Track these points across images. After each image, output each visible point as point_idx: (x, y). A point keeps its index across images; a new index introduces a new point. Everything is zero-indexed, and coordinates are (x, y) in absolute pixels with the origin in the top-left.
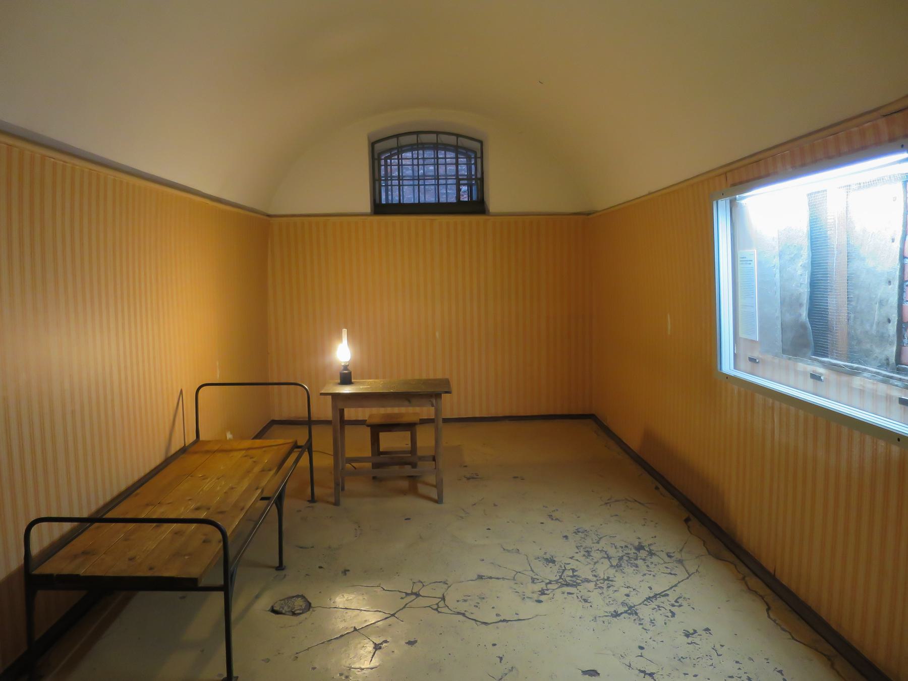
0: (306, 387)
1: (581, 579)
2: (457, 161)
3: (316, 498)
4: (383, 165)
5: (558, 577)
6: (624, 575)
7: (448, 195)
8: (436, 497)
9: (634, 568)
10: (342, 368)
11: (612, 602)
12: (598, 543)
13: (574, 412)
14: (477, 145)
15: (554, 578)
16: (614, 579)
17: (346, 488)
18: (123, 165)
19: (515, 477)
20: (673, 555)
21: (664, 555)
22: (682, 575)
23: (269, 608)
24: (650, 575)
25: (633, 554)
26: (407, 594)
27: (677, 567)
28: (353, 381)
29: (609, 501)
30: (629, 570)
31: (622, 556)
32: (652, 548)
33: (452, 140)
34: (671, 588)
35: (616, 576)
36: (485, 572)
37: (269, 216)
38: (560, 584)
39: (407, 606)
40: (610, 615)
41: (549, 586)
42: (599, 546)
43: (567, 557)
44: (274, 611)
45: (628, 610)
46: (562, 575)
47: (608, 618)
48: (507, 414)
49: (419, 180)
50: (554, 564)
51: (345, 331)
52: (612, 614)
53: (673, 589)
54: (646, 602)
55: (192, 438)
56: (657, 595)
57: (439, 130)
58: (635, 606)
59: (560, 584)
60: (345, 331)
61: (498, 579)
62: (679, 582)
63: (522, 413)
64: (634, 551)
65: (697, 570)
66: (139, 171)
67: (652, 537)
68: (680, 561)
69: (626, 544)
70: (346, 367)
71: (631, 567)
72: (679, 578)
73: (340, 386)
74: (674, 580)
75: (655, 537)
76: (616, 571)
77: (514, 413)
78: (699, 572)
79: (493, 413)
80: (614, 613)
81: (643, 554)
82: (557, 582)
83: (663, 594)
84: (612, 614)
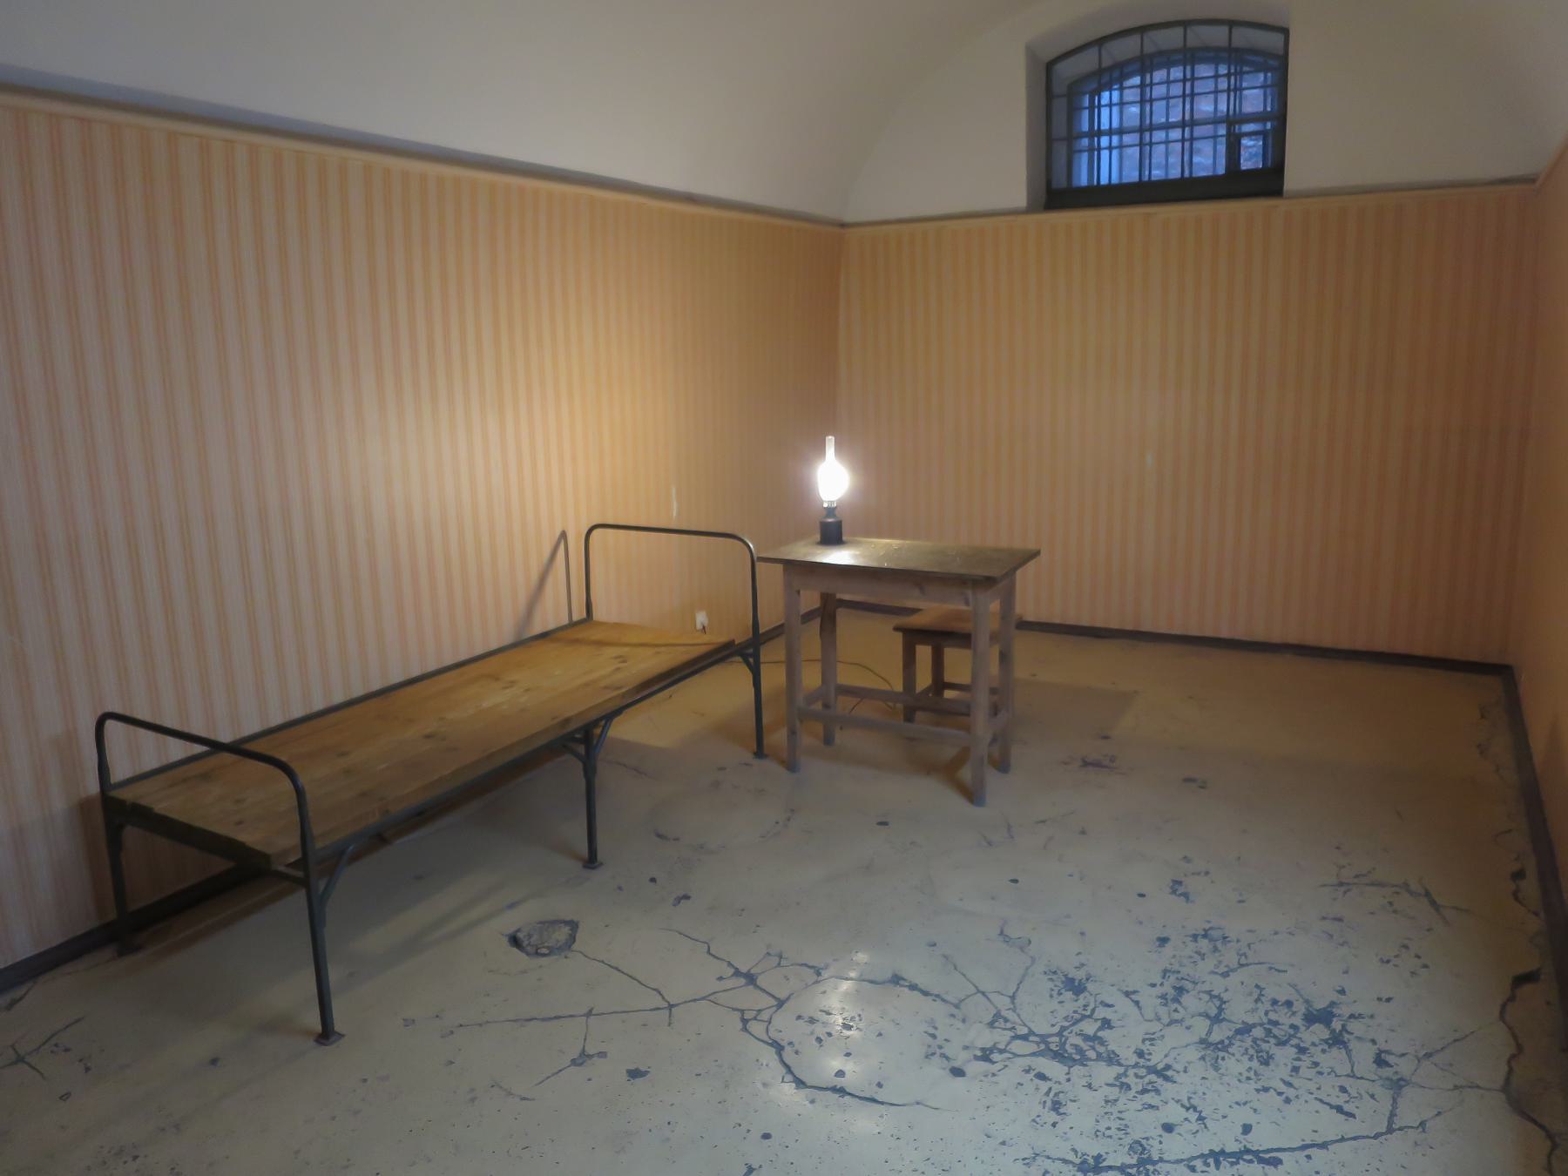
0: (751, 546)
1: (1101, 1049)
2: (1268, 86)
3: (766, 752)
4: (1086, 108)
5: (1056, 1029)
6: (1212, 1073)
7: (1208, 160)
8: (133, 836)
9: (1255, 1064)
10: (825, 513)
11: (1112, 1132)
12: (1225, 975)
13: (1456, 654)
14: (1275, 40)
15: (1042, 1028)
16: (1177, 1077)
17: (838, 740)
18: (1027, 178)
19: (1188, 780)
20: (1391, 1062)
21: (1364, 1055)
22: (1371, 1116)
23: (511, 930)
24: (1280, 1094)
25: (1286, 1028)
26: (737, 973)
27: (1372, 1096)
28: (844, 538)
29: (1356, 881)
30: (1236, 1064)
31: (1254, 1026)
32: (1353, 1026)
33: (1218, 36)
34: (1304, 1147)
35: (1189, 1069)
36: (912, 973)
37: (843, 225)
38: (1043, 1047)
39: (712, 998)
40: (1078, 1161)
41: (1018, 1047)
42: (1218, 985)
43: (1119, 990)
44: (515, 941)
45: (1131, 1166)
46: (1067, 1028)
47: (1065, 1168)
48: (1293, 638)
49: (1141, 130)
50: (1074, 997)
51: (830, 442)
52: (1084, 1162)
53: (1307, 1152)
54: (1198, 1164)
55: (579, 613)
56: (1248, 1151)
57: (1191, 16)
58: (1161, 1160)
59: (1043, 1047)
60: (830, 442)
61: (926, 993)
62: (1343, 1139)
63: (1327, 641)
64: (1298, 1021)
65: (1422, 1124)
66: (455, 151)
67: (1379, 999)
68: (1398, 1085)
69: (1293, 997)
70: (830, 511)
71: (1251, 1059)
72: (1351, 1128)
73: (820, 547)
74: (1332, 1125)
75: (1389, 1000)
76: (1203, 1058)
77: (1310, 639)
78: (1424, 1131)
79: (1259, 633)
80: (1091, 1161)
81: (1319, 1032)
82: (1044, 1038)
83: (1267, 1156)
84: (1084, 1162)
